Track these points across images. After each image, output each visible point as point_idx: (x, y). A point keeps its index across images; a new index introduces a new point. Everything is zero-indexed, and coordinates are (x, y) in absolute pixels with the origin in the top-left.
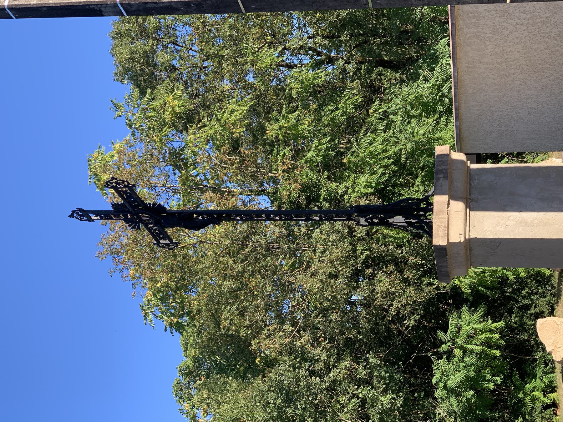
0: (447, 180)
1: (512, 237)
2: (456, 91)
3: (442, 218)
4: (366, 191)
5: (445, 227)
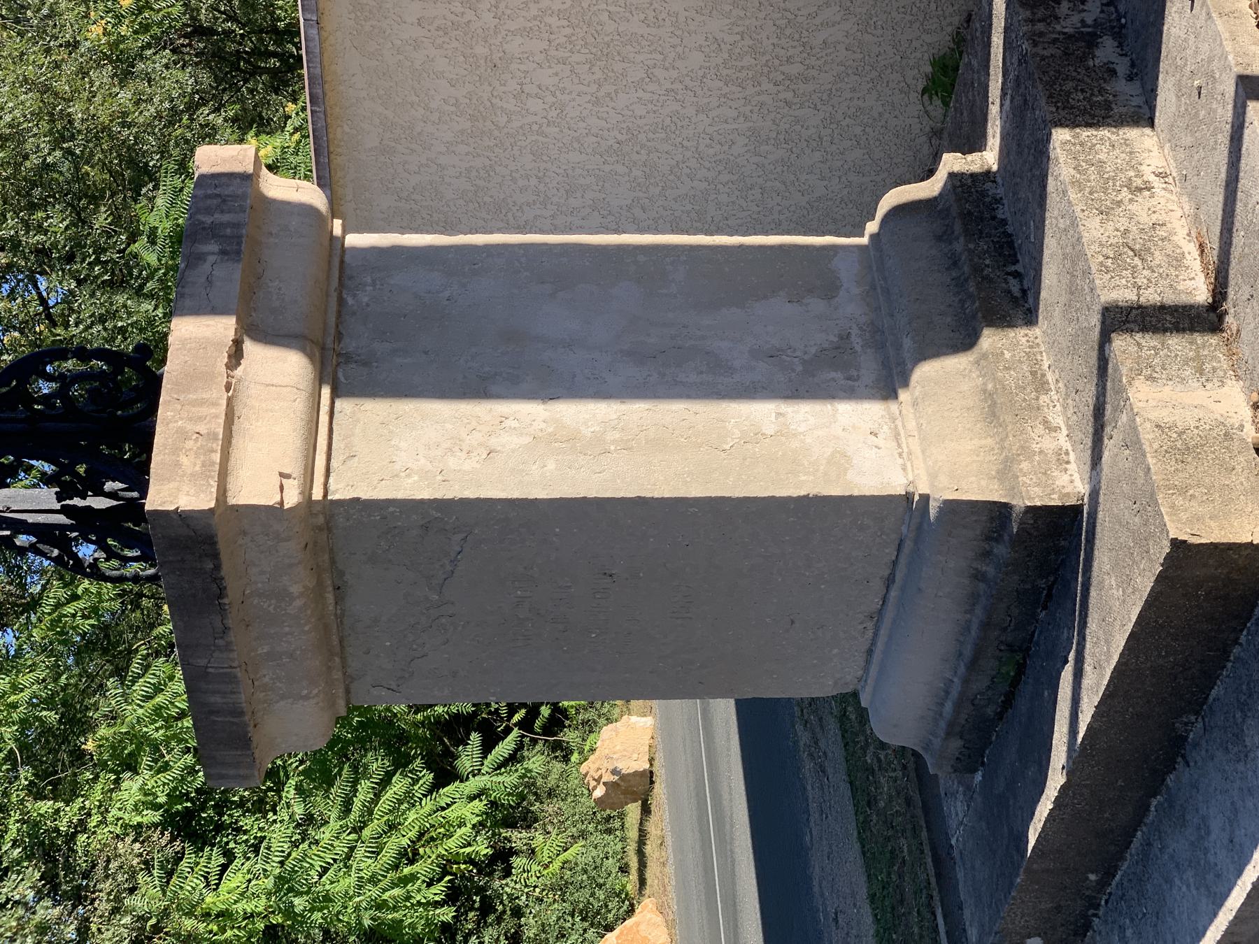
0: (238, 261)
1: (516, 494)
2: (321, 124)
3: (202, 402)
4: (137, 819)
5: (214, 437)
